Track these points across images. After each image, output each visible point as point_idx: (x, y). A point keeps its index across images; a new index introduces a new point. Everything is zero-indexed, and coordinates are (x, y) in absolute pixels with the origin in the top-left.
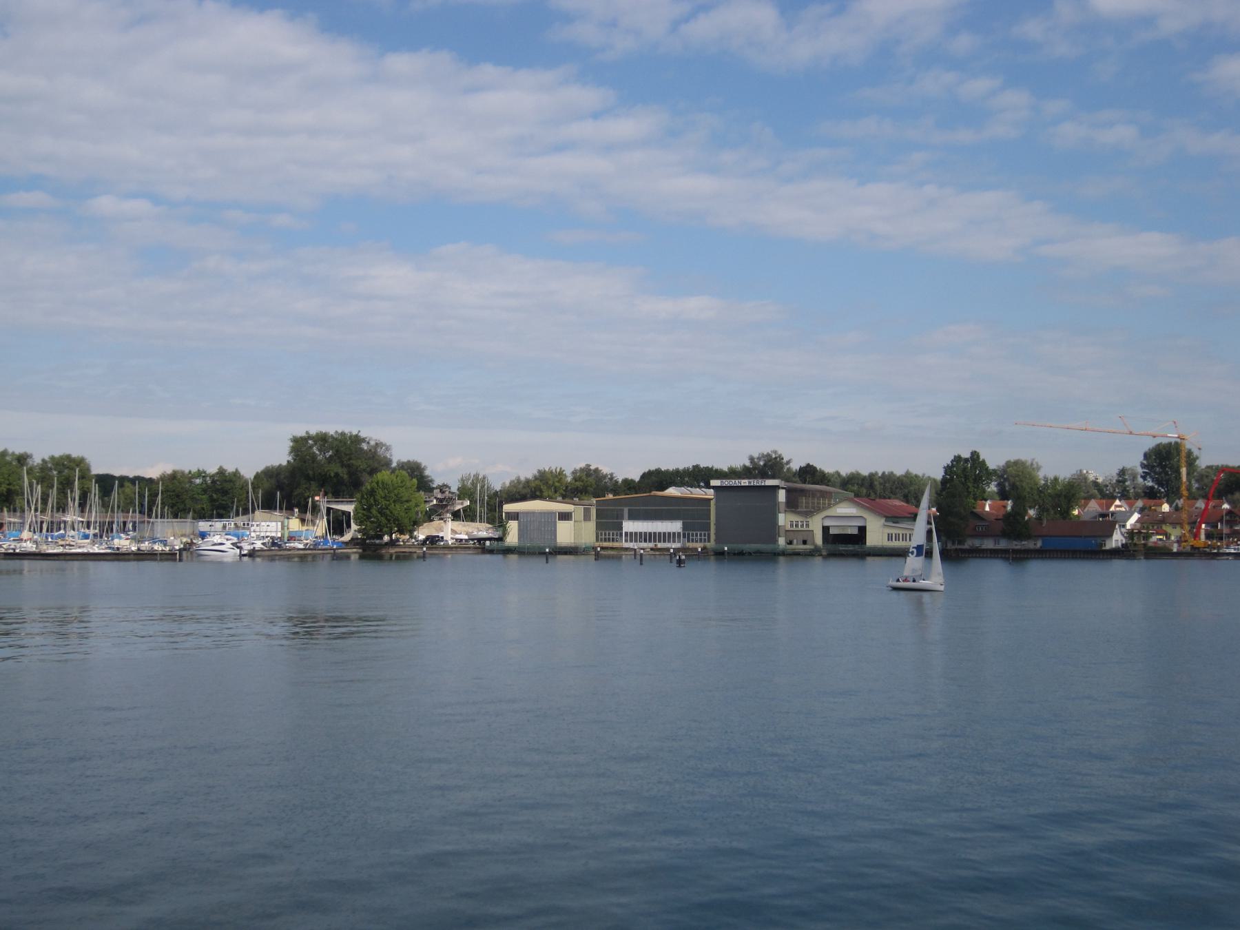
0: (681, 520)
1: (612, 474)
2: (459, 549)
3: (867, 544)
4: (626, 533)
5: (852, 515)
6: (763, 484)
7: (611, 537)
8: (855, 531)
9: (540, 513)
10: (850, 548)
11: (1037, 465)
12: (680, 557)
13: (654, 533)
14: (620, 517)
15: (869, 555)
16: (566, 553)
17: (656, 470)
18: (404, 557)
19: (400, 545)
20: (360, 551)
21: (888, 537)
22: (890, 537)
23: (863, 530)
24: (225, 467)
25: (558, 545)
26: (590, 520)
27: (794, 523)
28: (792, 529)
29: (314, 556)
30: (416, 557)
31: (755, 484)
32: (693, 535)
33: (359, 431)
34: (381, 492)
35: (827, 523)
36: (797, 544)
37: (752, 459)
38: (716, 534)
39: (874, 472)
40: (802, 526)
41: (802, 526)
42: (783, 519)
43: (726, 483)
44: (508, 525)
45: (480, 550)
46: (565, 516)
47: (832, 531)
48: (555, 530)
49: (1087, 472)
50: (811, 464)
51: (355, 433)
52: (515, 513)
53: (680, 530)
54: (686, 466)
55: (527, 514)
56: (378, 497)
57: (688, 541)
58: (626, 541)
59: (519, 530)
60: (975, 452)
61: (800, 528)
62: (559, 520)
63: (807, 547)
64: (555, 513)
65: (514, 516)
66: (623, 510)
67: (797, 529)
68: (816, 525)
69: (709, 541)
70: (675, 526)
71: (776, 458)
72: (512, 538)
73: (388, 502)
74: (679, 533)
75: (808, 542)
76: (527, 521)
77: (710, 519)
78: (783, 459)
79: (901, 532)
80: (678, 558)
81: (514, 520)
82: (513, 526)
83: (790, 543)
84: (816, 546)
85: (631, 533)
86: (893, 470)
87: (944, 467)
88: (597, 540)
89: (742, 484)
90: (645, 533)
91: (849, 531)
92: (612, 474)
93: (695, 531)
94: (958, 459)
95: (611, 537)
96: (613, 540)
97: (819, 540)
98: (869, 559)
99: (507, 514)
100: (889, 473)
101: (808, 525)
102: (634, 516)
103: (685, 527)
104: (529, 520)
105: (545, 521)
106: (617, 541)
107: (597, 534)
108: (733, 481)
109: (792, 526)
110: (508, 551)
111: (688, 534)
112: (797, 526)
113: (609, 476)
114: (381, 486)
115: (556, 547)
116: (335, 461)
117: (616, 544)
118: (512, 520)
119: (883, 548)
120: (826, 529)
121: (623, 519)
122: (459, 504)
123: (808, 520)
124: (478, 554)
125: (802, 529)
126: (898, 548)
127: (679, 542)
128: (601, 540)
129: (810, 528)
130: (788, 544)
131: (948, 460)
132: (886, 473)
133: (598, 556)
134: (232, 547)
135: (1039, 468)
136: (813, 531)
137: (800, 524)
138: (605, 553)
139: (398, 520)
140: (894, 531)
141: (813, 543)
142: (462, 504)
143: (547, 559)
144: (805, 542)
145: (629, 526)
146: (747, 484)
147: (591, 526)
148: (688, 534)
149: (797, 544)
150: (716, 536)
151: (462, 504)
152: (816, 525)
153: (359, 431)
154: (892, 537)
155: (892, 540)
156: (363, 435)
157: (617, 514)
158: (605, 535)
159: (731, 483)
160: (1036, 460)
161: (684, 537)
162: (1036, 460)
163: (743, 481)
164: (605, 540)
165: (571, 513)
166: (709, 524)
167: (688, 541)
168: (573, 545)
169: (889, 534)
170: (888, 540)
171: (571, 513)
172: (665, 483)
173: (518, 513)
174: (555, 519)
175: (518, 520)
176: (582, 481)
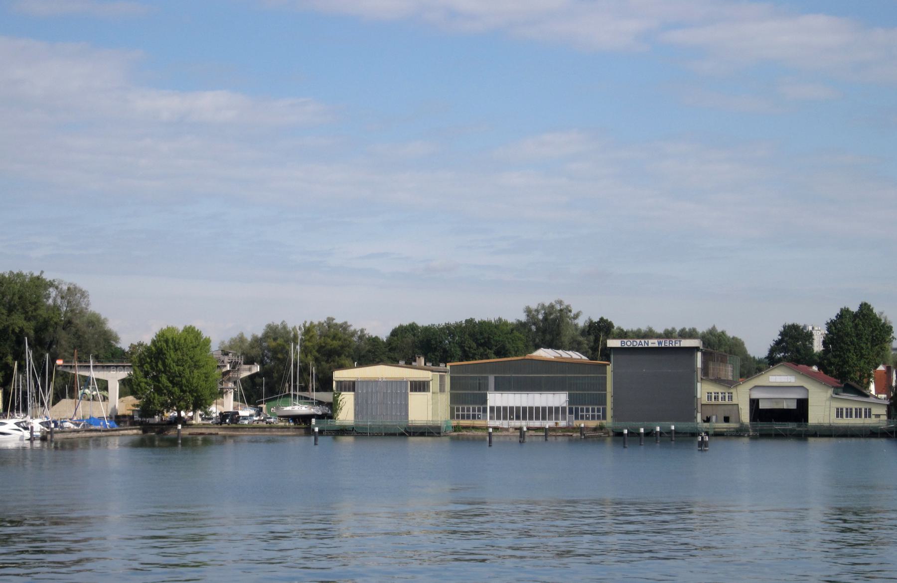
0: (565, 390)
1: (362, 331)
2: (274, 430)
3: (809, 422)
4: (492, 408)
5: (782, 385)
6: (677, 345)
7: (471, 413)
8: (793, 406)
9: (387, 382)
10: (791, 426)
11: (885, 320)
12: (702, 438)
13: (549, 408)
14: (483, 387)
15: (815, 435)
16: (422, 434)
17: (410, 325)
18: (188, 443)
19: (192, 425)
20: (140, 432)
21: (837, 412)
22: (839, 413)
23: (803, 404)
24: (313, 321)
25: (410, 424)
26: (444, 391)
27: (713, 395)
28: (709, 402)
29: (86, 440)
30: (200, 442)
31: (668, 345)
32: (582, 410)
33: (42, 272)
34: (173, 356)
35: (756, 395)
36: (717, 421)
37: (528, 311)
38: (614, 409)
39: (670, 329)
40: (724, 398)
41: (724, 398)
42: (704, 391)
43: (628, 343)
44: (340, 398)
45: (303, 431)
46: (420, 386)
47: (763, 405)
48: (407, 405)
49: (813, 328)
50: (605, 318)
51: (36, 274)
52: (350, 381)
53: (565, 405)
54: (458, 321)
55: (367, 382)
56: (169, 361)
57: (577, 418)
58: (491, 418)
59: (357, 403)
60: (866, 304)
61: (720, 401)
62: (411, 391)
63: (732, 425)
64: (407, 382)
65: (350, 386)
66: (486, 378)
67: (717, 403)
68: (742, 397)
69: (604, 417)
70: (559, 399)
71: (561, 310)
72: (346, 414)
73: (181, 368)
74: (564, 409)
75: (730, 419)
76: (367, 392)
77: (606, 390)
78: (570, 311)
79: (863, 407)
80: (700, 440)
81: (349, 391)
82: (347, 400)
83: (708, 420)
84: (742, 424)
85: (499, 408)
86: (697, 328)
87: (827, 324)
88: (452, 417)
89: (650, 345)
90: (518, 408)
91: (785, 406)
92: (362, 331)
93: (585, 404)
94: (844, 314)
95: (471, 413)
96: (474, 417)
97: (745, 417)
98: (811, 440)
99: (339, 383)
100: (690, 329)
101: (731, 398)
102: (501, 386)
103: (572, 400)
104: (370, 390)
105: (392, 392)
106: (479, 418)
107: (452, 410)
108: (638, 341)
109: (709, 398)
110: (343, 431)
111: (577, 410)
112: (716, 398)
113: (359, 333)
114: (172, 347)
115: (409, 427)
116: (18, 310)
117: (477, 423)
118: (345, 391)
119: (848, 427)
120: (754, 403)
121: (487, 390)
122: (245, 370)
123: (731, 391)
124: (300, 435)
125: (723, 402)
126: (854, 427)
127: (565, 419)
128: (458, 417)
129: (735, 401)
130: (705, 421)
131: (832, 315)
132: (687, 330)
133: (453, 439)
134: (17, 427)
135: (350, 326)
136: (738, 404)
137: (720, 396)
138: (469, 434)
139: (196, 391)
140: (844, 405)
141: (738, 420)
142: (250, 370)
143: (316, 440)
144: (727, 420)
145: (495, 399)
146: (656, 345)
147: (445, 399)
148: (577, 410)
149: (717, 421)
150: (614, 412)
151: (250, 370)
152: (742, 397)
153: (42, 272)
154: (842, 412)
155: (842, 417)
156: (48, 277)
157: (479, 383)
158: (463, 410)
159: (635, 343)
160: (884, 315)
161: (571, 412)
162: (884, 315)
163: (651, 341)
164: (463, 417)
165: (428, 382)
166: (605, 395)
167: (577, 418)
168: (430, 424)
169: (837, 409)
170: (837, 416)
171: (428, 382)
172: (433, 342)
173: (354, 383)
174: (407, 389)
175: (354, 390)
176: (340, 339)
